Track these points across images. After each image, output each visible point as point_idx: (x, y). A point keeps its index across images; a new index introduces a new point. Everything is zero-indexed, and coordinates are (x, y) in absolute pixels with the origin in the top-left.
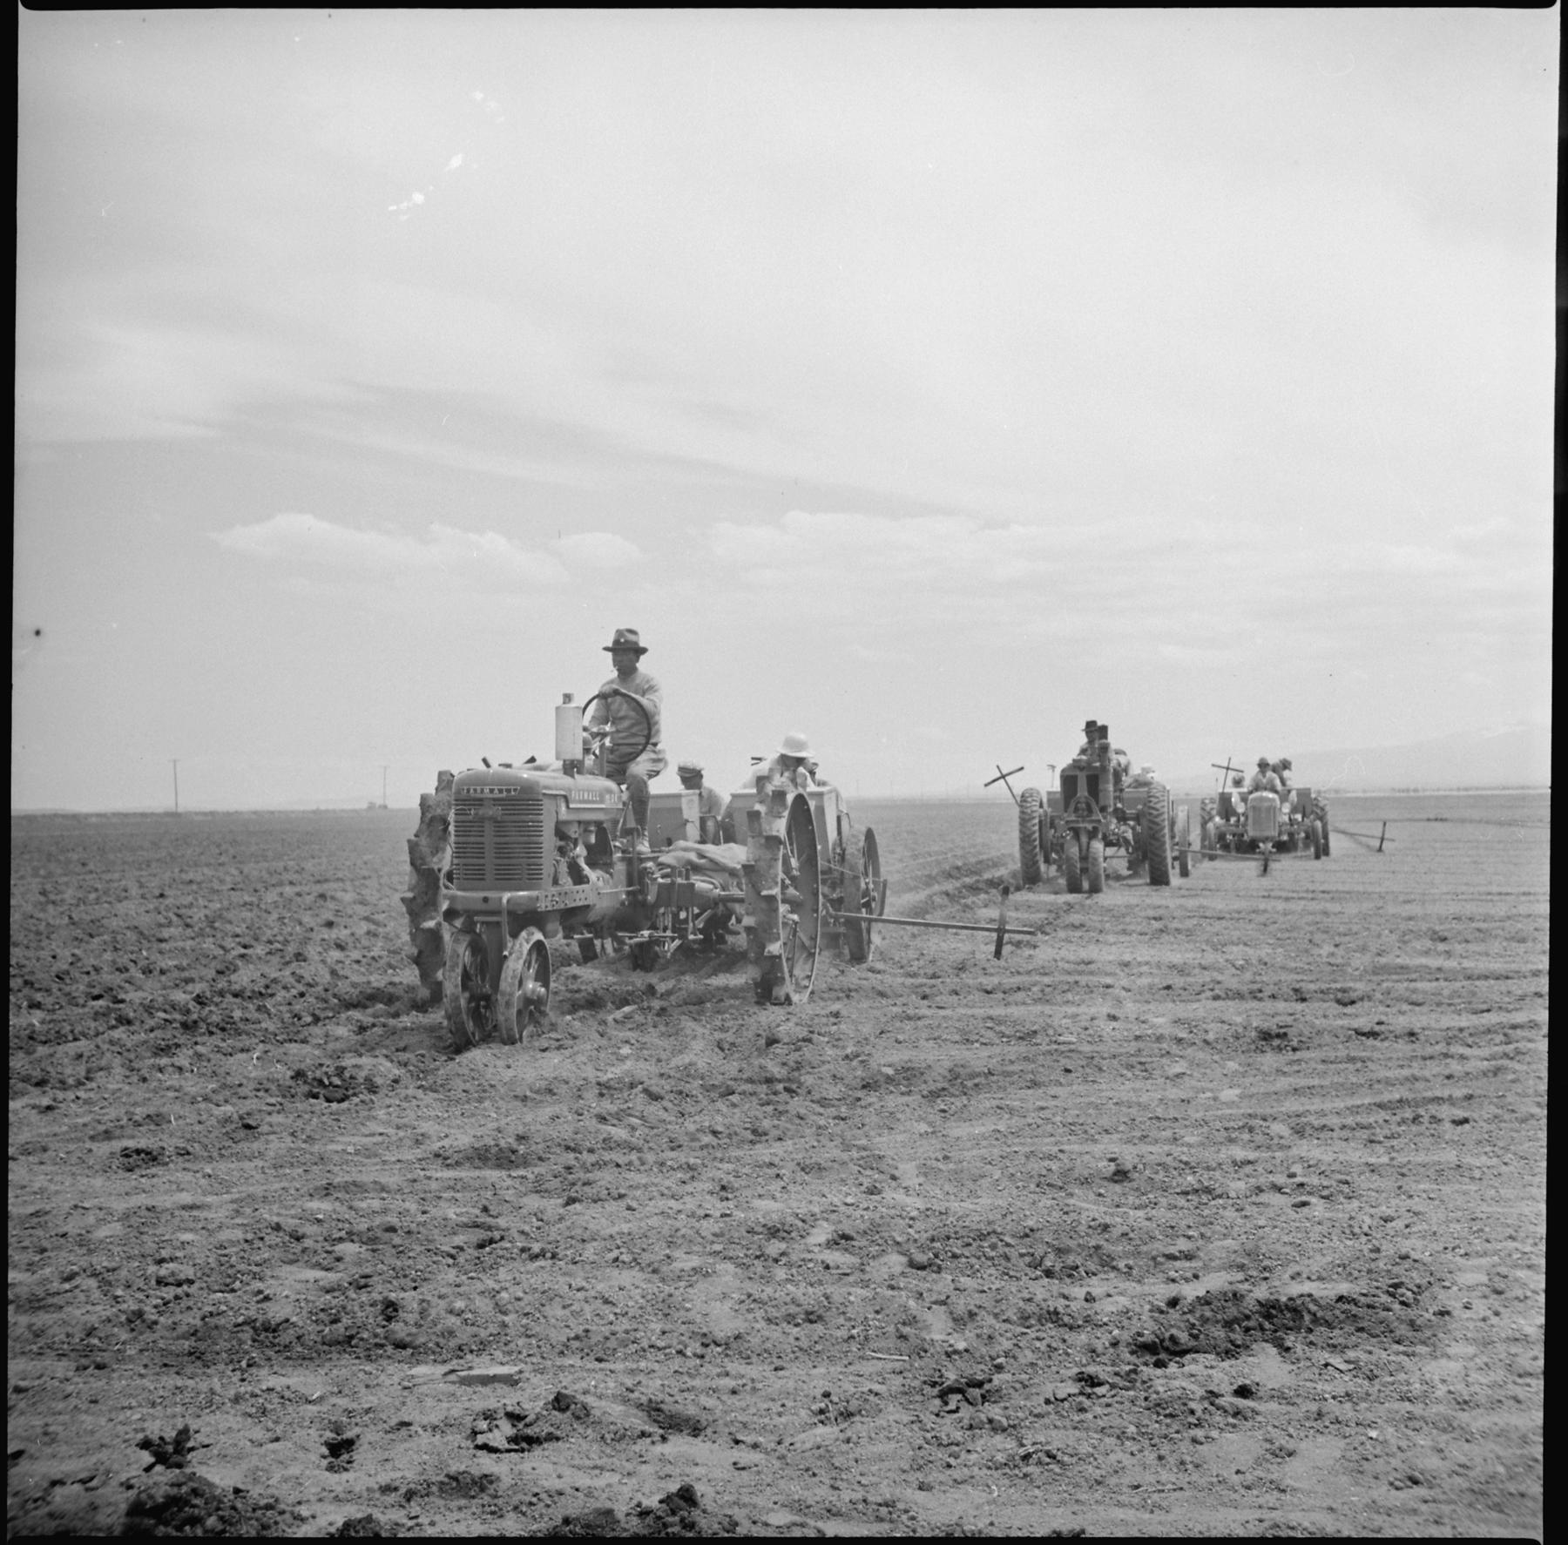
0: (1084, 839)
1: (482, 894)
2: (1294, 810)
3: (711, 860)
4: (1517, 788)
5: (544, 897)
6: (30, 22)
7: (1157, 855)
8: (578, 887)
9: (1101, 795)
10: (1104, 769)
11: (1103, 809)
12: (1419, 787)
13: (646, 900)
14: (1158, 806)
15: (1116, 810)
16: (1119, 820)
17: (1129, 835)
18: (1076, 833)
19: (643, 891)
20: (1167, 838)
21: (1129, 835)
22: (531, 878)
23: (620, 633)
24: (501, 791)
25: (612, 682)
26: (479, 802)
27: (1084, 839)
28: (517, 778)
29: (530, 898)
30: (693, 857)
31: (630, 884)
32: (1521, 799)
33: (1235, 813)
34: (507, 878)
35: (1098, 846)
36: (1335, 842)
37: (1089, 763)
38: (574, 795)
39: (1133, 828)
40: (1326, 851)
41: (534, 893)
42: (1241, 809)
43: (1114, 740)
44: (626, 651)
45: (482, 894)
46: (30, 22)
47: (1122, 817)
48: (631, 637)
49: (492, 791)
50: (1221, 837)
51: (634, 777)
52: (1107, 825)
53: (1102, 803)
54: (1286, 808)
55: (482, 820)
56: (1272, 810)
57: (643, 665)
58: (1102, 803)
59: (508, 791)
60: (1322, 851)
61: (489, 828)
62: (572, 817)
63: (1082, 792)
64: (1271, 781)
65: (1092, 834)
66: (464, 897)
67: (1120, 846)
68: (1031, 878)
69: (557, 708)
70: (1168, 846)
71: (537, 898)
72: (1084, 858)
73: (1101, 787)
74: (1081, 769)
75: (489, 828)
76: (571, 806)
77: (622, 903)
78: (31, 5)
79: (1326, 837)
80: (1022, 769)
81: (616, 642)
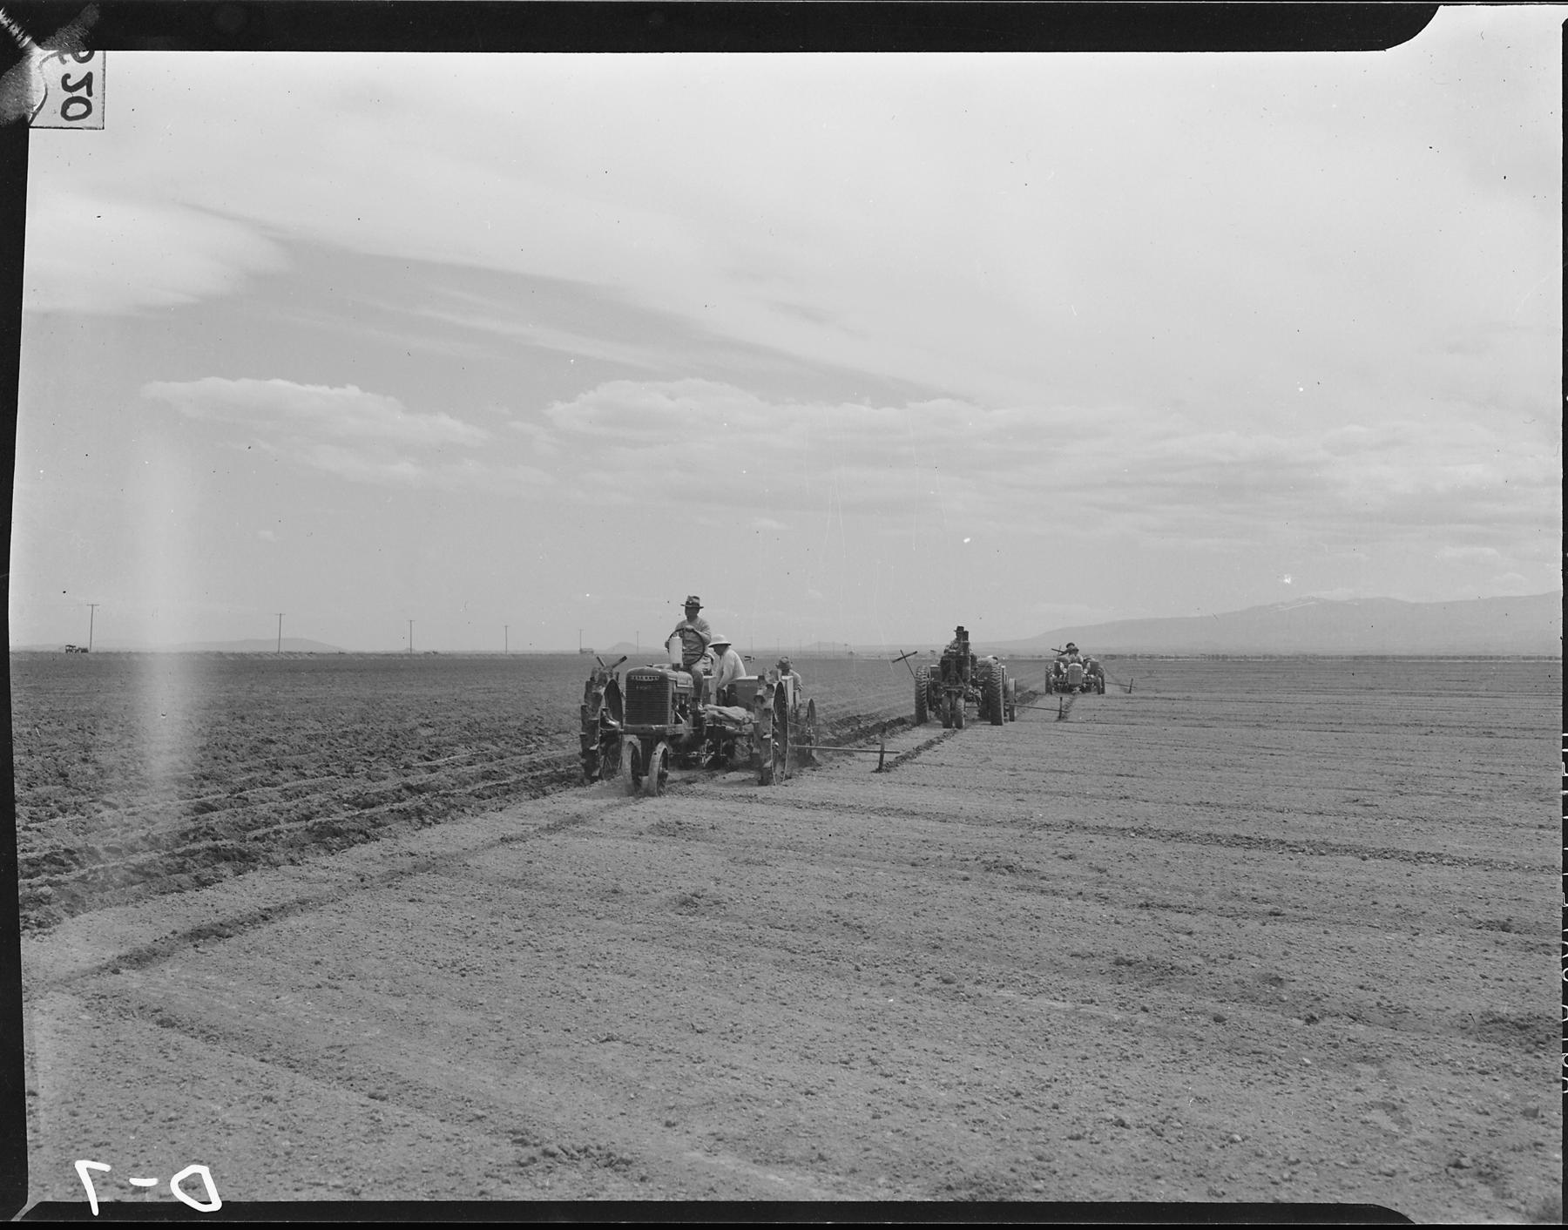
2: (1089, 673)
3: (726, 715)
4: (1545, 658)
10: (965, 658)
11: (965, 681)
15: (972, 680)
16: (974, 686)
17: (979, 695)
18: (949, 694)
19: (701, 730)
20: (1001, 698)
21: (979, 695)
23: (690, 598)
25: (684, 622)
27: (953, 698)
30: (716, 713)
31: (694, 725)
33: (1062, 673)
35: (961, 702)
36: (1108, 689)
37: (958, 653)
38: (679, 681)
39: (981, 691)
40: (1103, 692)
41: (665, 726)
42: (1065, 671)
43: (971, 639)
44: (692, 608)
47: (975, 684)
48: (695, 600)
50: (1056, 683)
51: (697, 672)
52: (967, 689)
54: (1086, 671)
56: (1079, 672)
57: (700, 614)
60: (1101, 691)
62: (679, 691)
63: (953, 672)
65: (958, 696)
68: (921, 719)
70: (1002, 704)
72: (953, 707)
79: (1103, 685)
81: (687, 603)
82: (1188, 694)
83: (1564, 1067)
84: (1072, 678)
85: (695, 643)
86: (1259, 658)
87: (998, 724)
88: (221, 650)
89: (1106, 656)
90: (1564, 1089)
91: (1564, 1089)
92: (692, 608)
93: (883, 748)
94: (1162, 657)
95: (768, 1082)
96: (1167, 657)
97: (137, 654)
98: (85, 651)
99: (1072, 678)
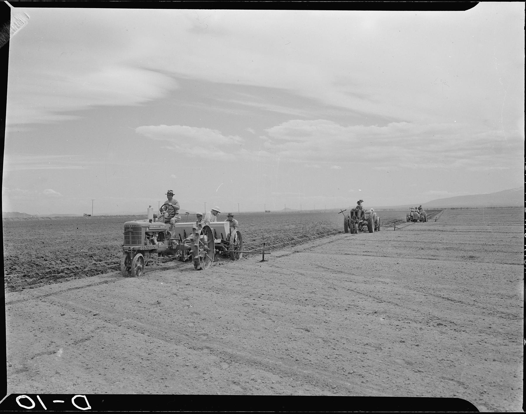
0: (354, 223)
1: (129, 247)
5: (142, 247)
6: (524, 2)
7: (371, 227)
8: (154, 245)
9: (358, 215)
12: (74, 280)
13: (172, 248)
14: (371, 218)
22: (140, 243)
24: (132, 226)
25: (167, 201)
26: (128, 228)
27: (354, 223)
28: (137, 223)
29: (139, 247)
32: (511, 210)
34: (134, 243)
44: (170, 195)
45: (129, 247)
46: (524, 2)
48: (171, 192)
49: (131, 226)
53: (358, 217)
55: (129, 232)
56: (417, 215)
57: (174, 197)
58: (358, 217)
59: (134, 226)
61: (130, 233)
63: (354, 215)
64: (417, 211)
66: (125, 247)
67: (365, 225)
69: (148, 209)
71: (140, 247)
73: (358, 214)
74: (354, 211)
75: (130, 233)
76: (150, 229)
77: (167, 249)
78: (16, 5)
80: (346, 210)
82: (453, 227)
83: (525, 237)
84: (414, 217)
85: (172, 209)
86: (507, 208)
87: (371, 232)
88: (134, 215)
89: (451, 209)
90: (525, 249)
91: (525, 249)
92: (170, 195)
93: (395, 226)
94: (471, 208)
95: (99, 365)
96: (473, 208)
97: (231, 213)
98: (89, 216)
99: (414, 217)
